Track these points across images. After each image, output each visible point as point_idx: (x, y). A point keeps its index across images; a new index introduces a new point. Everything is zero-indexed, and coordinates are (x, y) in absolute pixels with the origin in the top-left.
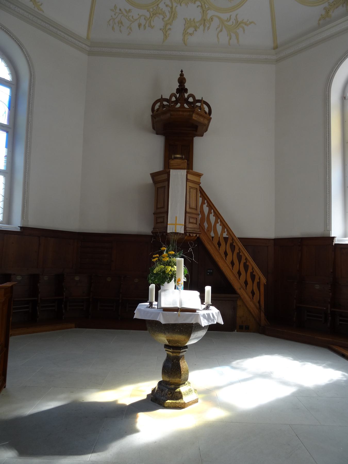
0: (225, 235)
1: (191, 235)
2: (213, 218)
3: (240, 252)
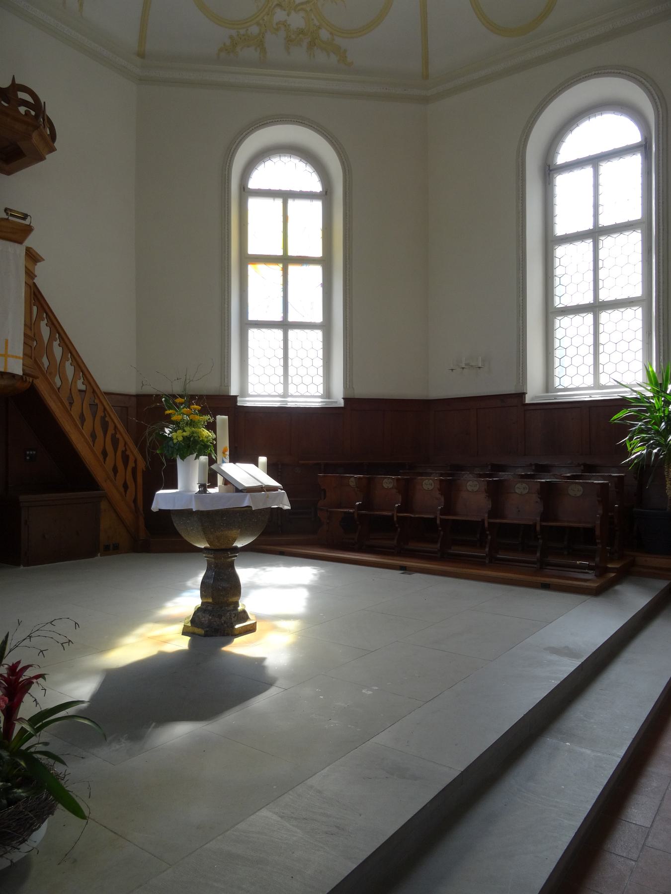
0: (80, 385)
2: (58, 351)
3: (105, 416)
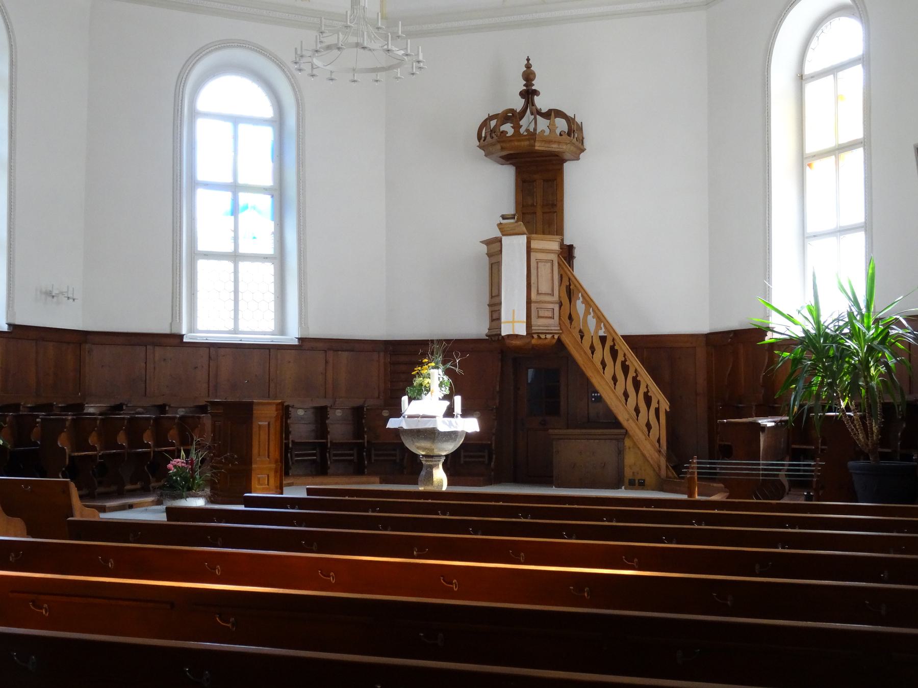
0: (602, 333)
1: (543, 336)
3: (626, 360)
